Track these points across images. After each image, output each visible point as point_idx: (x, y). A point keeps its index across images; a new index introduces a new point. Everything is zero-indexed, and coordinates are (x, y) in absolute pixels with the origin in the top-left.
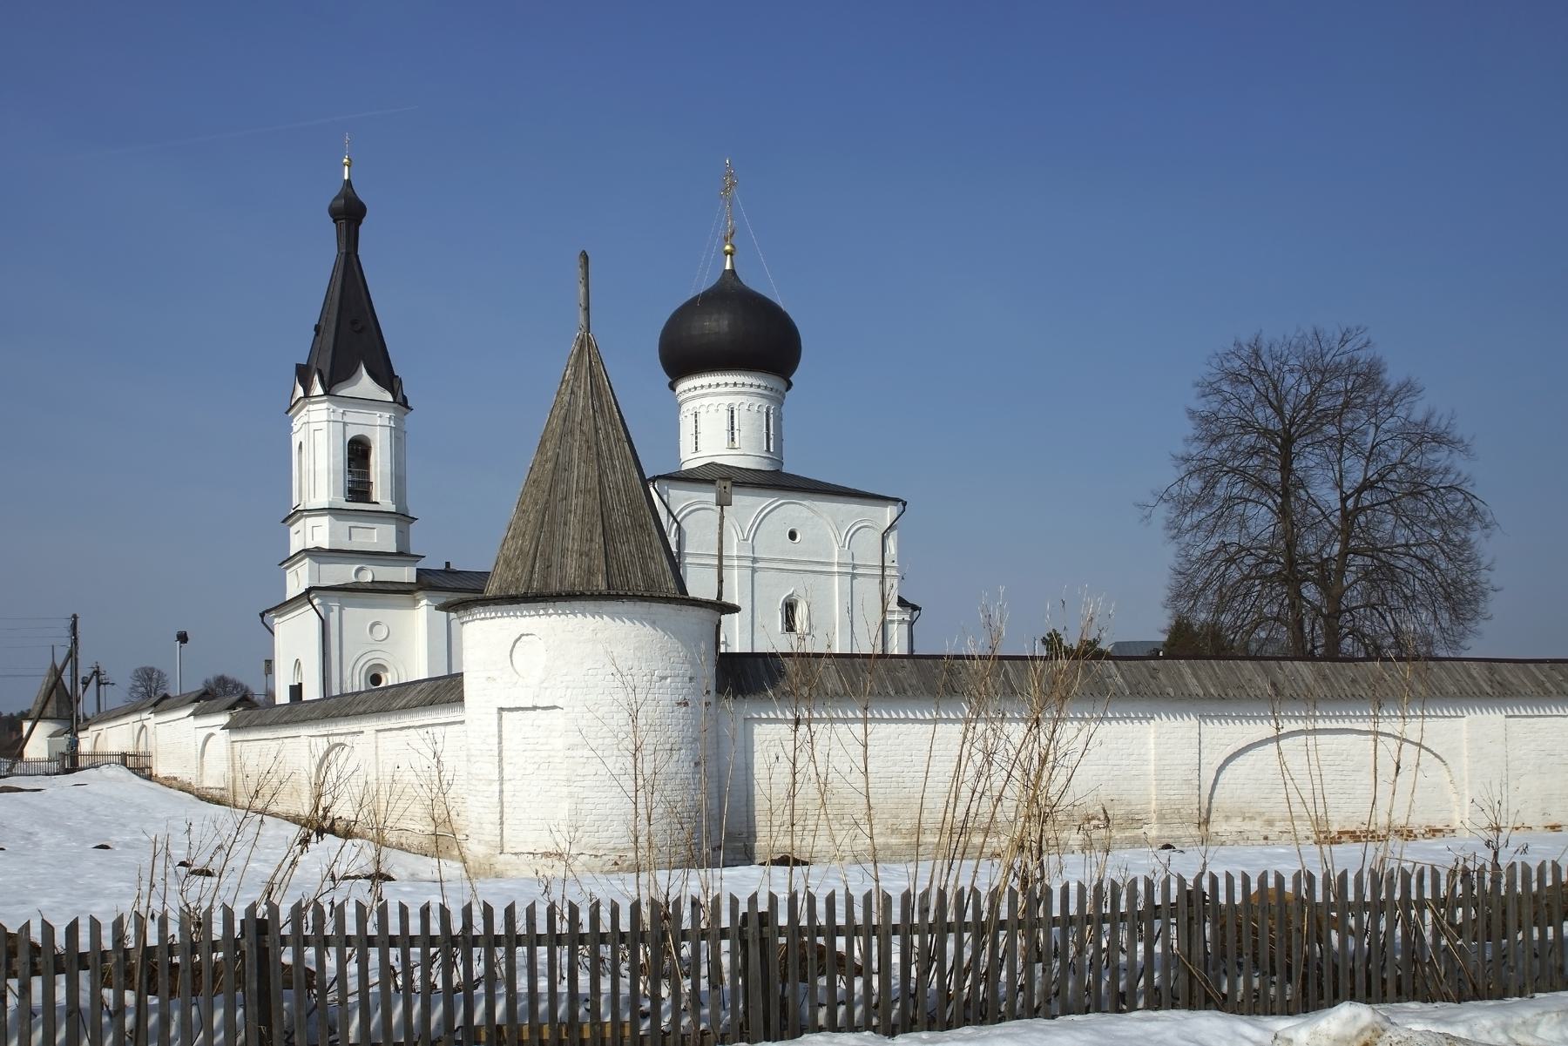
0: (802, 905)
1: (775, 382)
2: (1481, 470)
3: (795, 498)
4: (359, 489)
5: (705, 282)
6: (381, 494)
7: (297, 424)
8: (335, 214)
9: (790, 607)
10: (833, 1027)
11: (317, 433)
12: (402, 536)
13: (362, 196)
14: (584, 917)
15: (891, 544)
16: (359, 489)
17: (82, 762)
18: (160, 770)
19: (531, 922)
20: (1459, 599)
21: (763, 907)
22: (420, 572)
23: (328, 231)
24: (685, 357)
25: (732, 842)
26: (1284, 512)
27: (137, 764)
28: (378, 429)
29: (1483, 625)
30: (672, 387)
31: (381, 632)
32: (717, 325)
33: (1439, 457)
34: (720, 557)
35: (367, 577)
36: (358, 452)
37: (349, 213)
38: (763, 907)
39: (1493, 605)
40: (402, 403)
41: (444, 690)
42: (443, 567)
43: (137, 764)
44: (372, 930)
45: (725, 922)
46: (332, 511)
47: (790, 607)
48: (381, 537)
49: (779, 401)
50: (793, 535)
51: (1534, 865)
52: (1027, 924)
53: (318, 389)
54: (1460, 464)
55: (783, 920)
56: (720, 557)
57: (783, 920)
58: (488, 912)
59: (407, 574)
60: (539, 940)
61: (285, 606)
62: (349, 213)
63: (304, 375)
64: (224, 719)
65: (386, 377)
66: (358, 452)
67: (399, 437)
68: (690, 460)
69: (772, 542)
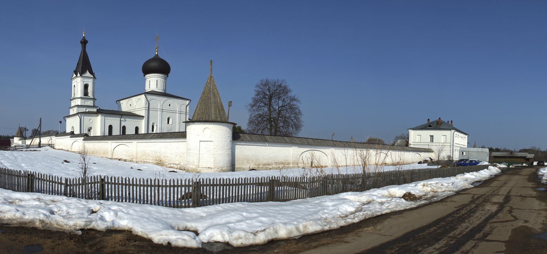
0: (135, 180)
1: (165, 76)
3: (170, 98)
4: (86, 94)
5: (152, 56)
6: (90, 94)
7: (73, 81)
8: (81, 43)
9: (168, 119)
11: (78, 83)
12: (94, 103)
13: (87, 39)
14: (180, 182)
15: (188, 108)
16: (86, 94)
18: (56, 147)
19: (122, 181)
21: (198, 181)
22: (97, 110)
24: (147, 70)
25: (233, 168)
28: (90, 82)
32: (154, 64)
34: (148, 110)
35: (87, 110)
37: (84, 42)
38: (198, 181)
40: (94, 77)
41: (182, 135)
42: (426, 122)
43: (51, 146)
44: (164, 184)
45: (191, 184)
46: (81, 98)
47: (168, 119)
48: (90, 103)
49: (166, 79)
51: (260, 178)
52: (84, 181)
53: (79, 75)
56: (148, 110)
58: (210, 180)
59: (95, 110)
60: (112, 184)
61: (69, 116)
62: (84, 42)
63: (76, 73)
64: (83, 138)
65: (91, 73)
66: (86, 87)
67: (94, 83)
68: (148, 89)
69: (166, 107)
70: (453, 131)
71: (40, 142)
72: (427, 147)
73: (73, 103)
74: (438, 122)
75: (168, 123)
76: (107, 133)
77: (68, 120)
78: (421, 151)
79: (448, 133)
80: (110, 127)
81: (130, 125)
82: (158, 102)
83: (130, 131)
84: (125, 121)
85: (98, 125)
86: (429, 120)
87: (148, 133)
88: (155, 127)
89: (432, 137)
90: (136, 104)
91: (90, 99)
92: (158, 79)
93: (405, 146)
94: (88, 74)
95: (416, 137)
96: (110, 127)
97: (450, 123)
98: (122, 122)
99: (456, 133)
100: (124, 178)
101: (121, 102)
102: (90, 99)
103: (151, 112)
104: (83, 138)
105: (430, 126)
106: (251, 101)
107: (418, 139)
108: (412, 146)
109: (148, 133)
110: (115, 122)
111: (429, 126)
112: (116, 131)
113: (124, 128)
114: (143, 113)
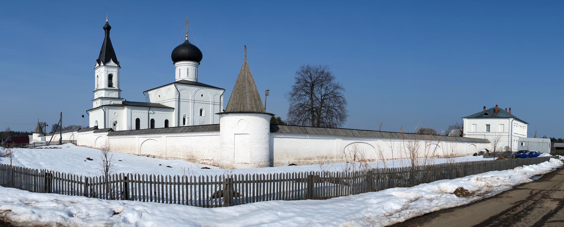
1: (197, 63)
2: (346, 94)
4: (110, 85)
6: (115, 85)
7: (96, 71)
8: (104, 28)
9: (201, 111)
10: (216, 206)
11: (101, 73)
12: (119, 94)
16: (110, 85)
17: (62, 142)
20: (342, 117)
22: (123, 102)
23: (103, 32)
24: (177, 57)
26: (311, 99)
27: (74, 142)
28: (114, 72)
29: (346, 122)
30: (174, 64)
31: (116, 115)
32: (184, 51)
33: (338, 91)
35: (112, 103)
36: (110, 77)
37: (108, 28)
39: (348, 119)
41: (216, 128)
42: (482, 110)
43: (74, 142)
44: (168, 181)
47: (201, 111)
48: (115, 95)
49: (197, 67)
50: (202, 96)
53: (102, 64)
54: (342, 92)
55: (130, 179)
57: (130, 179)
58: (243, 176)
59: (120, 102)
61: (92, 109)
62: (108, 28)
63: (99, 61)
64: (107, 133)
65: (116, 61)
66: (110, 77)
67: (118, 73)
68: (178, 79)
70: (511, 119)
71: (61, 138)
72: (483, 137)
73: (97, 95)
74: (494, 110)
75: (201, 115)
76: (134, 127)
77: (91, 114)
78: (477, 142)
79: (506, 122)
80: (138, 121)
81: (159, 118)
82: (189, 92)
83: (159, 124)
84: (154, 113)
85: (124, 118)
86: (485, 107)
87: (179, 127)
88: (186, 119)
89: (488, 126)
90: (165, 95)
91: (115, 90)
92: (189, 67)
93: (459, 136)
94: (112, 63)
95: (472, 127)
96: (138, 121)
97: (508, 111)
98: (150, 115)
99: (515, 121)
100: (279, 174)
101: (149, 92)
102: (115, 90)
103: (181, 103)
104: (107, 133)
105: (486, 114)
106: (291, 90)
107: (473, 129)
108: (466, 136)
109: (179, 127)
110: (143, 115)
111: (485, 115)
112: (144, 125)
113: (153, 121)
114: (173, 104)
